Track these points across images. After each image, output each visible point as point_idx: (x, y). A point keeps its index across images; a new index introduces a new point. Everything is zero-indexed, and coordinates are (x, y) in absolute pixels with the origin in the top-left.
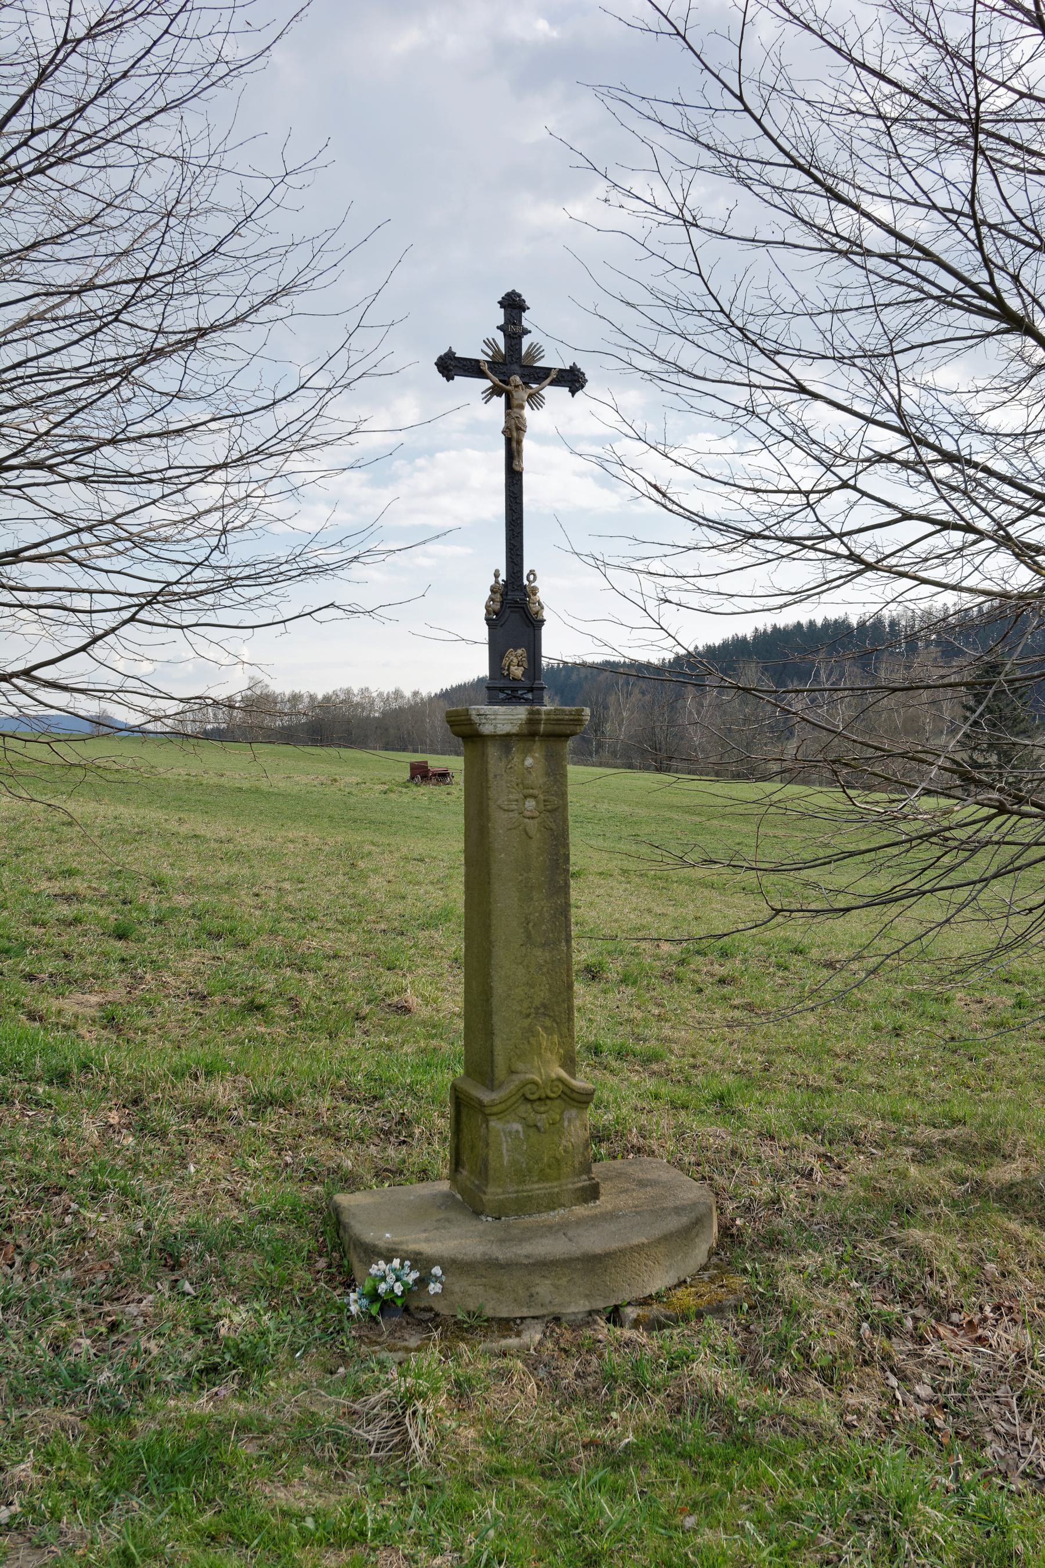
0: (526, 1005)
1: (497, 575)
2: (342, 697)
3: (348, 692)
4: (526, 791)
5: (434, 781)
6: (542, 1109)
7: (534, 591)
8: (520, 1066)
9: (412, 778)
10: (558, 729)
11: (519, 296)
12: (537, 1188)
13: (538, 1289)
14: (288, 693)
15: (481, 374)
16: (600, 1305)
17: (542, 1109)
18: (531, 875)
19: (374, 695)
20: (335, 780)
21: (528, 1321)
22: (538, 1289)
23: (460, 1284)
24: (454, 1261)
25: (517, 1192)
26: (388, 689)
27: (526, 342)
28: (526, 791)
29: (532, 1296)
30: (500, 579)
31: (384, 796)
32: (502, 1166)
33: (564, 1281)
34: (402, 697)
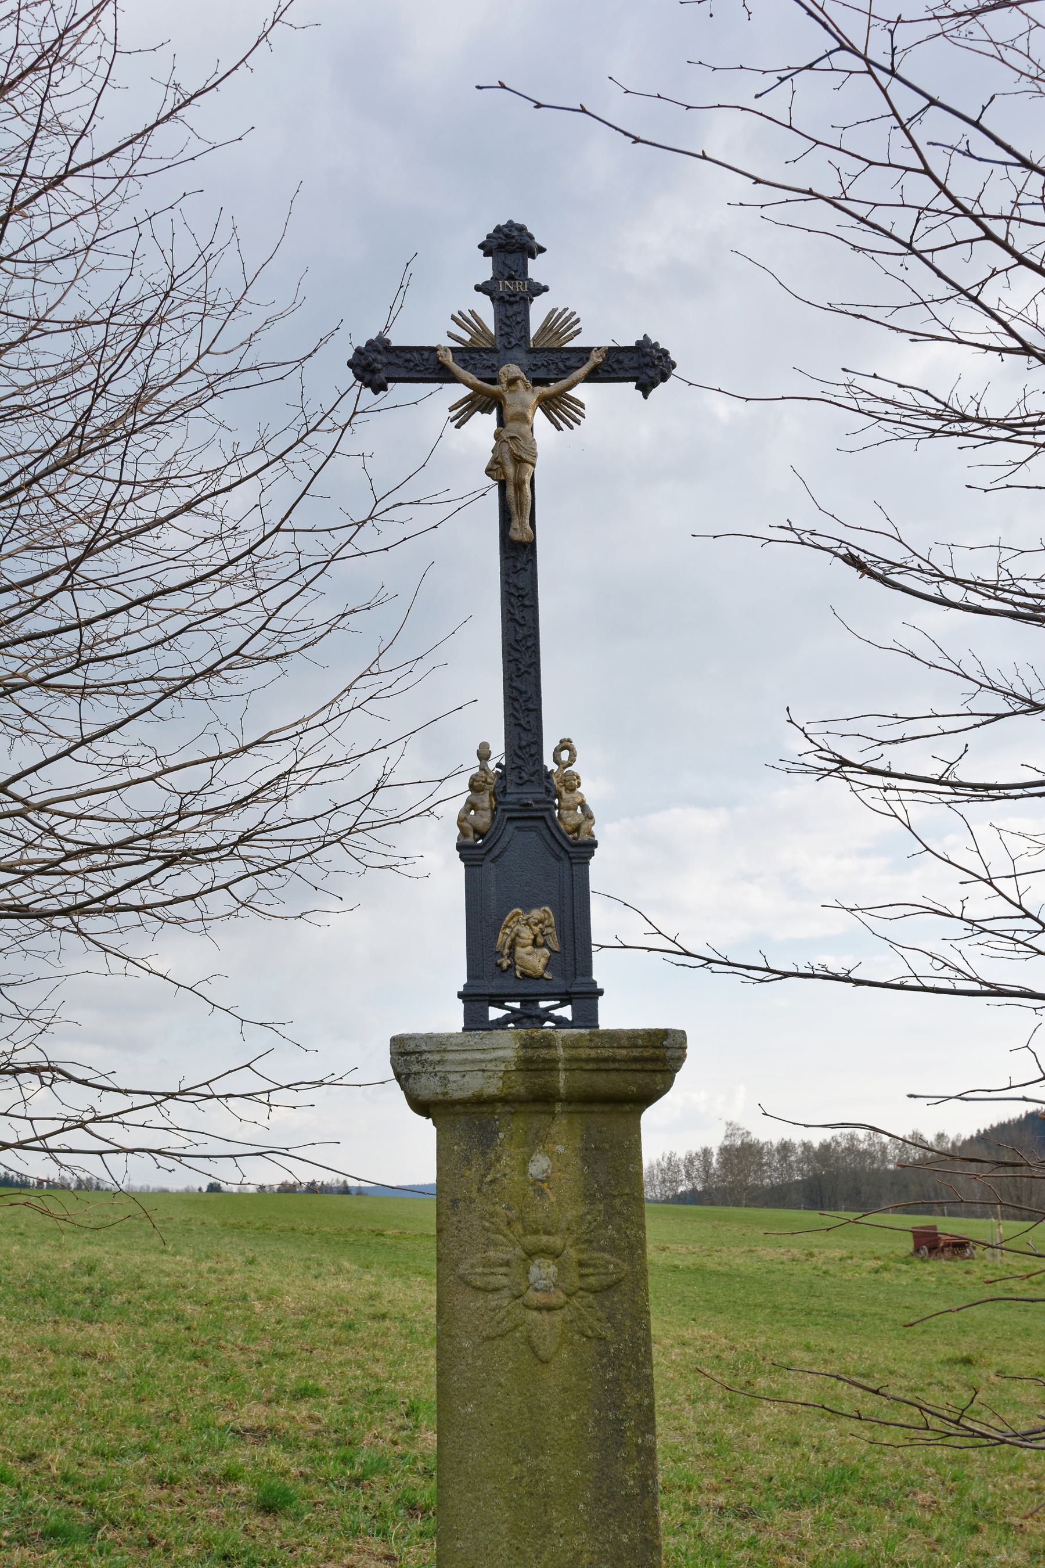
1: (484, 754)
2: (844, 1144)
4: (530, 1240)
5: (948, 1254)
7: (571, 783)
9: (917, 1250)
10: (603, 1082)
11: (522, 229)
14: (776, 1142)
15: (444, 375)
20: (811, 1255)
27: (538, 312)
28: (530, 1240)
30: (491, 765)
31: (873, 1276)
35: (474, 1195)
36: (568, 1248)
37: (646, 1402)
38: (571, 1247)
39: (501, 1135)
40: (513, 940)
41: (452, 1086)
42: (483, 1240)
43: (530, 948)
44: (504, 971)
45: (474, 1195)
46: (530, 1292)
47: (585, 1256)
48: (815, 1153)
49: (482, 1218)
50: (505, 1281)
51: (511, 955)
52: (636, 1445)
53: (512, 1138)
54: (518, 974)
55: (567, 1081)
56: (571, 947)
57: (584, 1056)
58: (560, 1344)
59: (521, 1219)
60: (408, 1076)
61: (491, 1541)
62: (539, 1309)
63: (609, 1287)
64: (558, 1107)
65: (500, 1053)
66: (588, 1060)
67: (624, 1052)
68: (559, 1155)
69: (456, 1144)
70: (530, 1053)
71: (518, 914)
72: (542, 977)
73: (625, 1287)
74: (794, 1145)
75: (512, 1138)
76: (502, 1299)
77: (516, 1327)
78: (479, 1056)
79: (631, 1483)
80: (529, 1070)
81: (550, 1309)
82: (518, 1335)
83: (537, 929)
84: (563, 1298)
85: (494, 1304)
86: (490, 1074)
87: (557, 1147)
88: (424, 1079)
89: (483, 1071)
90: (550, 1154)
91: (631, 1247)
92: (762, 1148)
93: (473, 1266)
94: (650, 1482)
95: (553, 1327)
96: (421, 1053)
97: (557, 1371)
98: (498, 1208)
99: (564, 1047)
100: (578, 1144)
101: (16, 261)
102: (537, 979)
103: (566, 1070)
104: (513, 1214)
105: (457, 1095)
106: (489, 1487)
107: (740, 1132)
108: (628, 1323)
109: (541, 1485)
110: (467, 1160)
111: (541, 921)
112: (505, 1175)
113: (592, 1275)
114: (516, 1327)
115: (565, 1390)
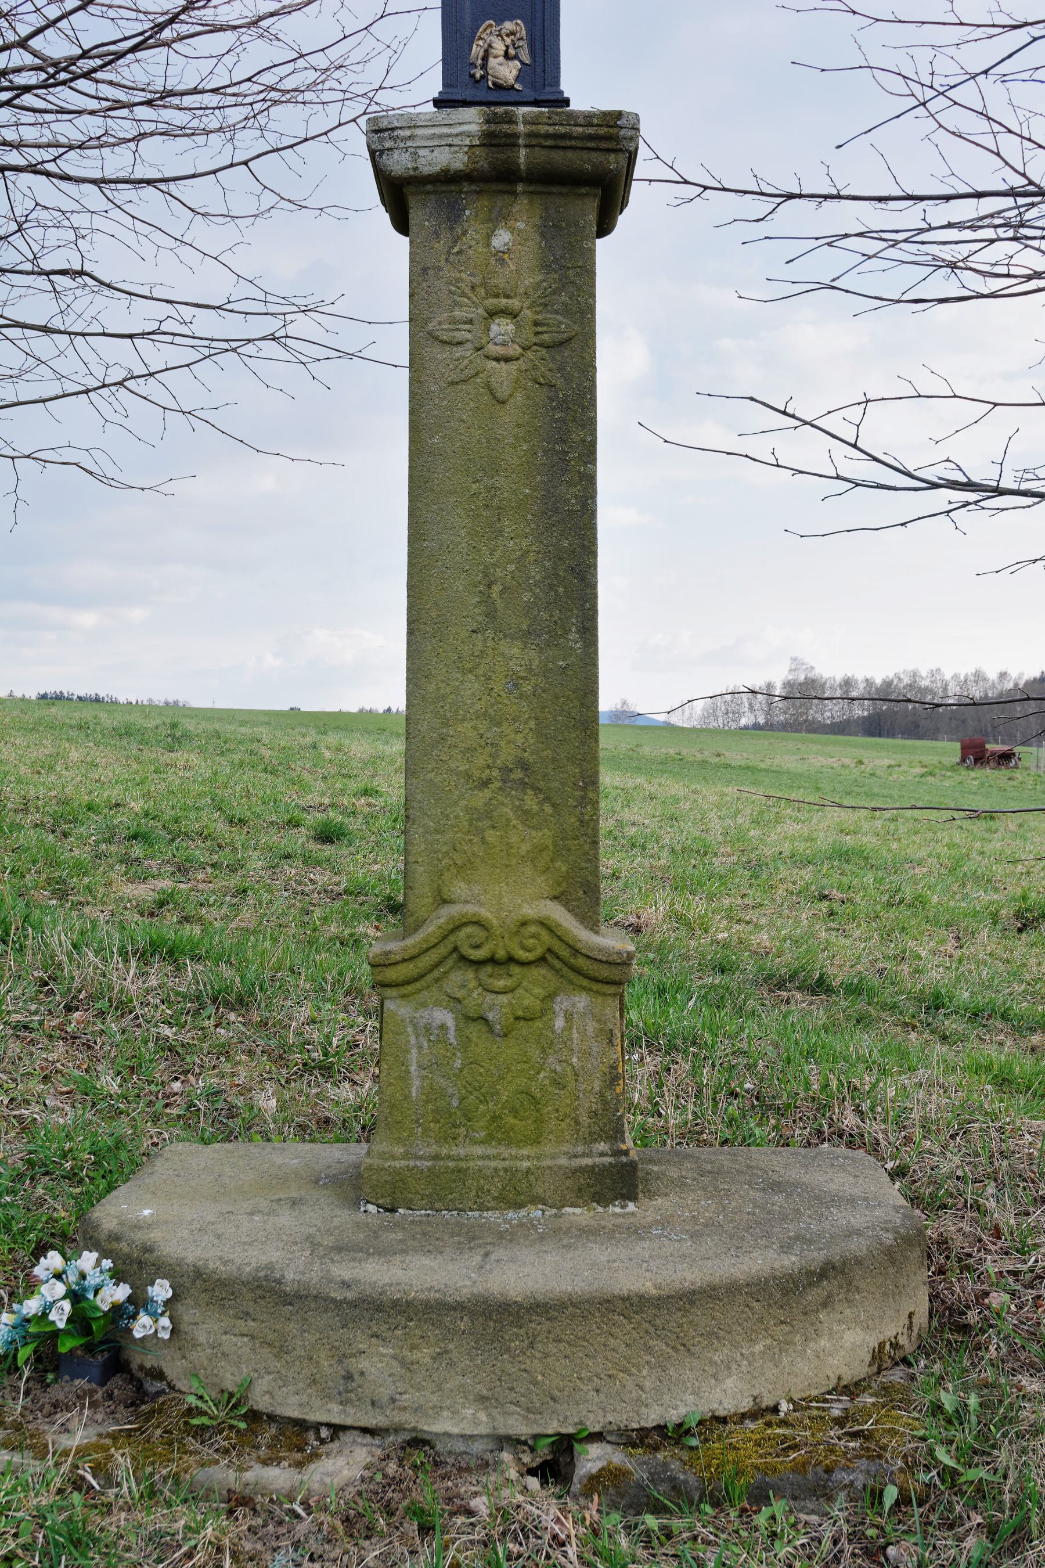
0: (481, 760)
2: (906, 681)
3: (915, 674)
6: (501, 984)
8: (459, 888)
12: (475, 1153)
13: (363, 1364)
16: (520, 1428)
17: (501, 984)
18: (500, 481)
19: (948, 677)
21: (347, 1437)
22: (363, 1364)
23: (207, 1327)
24: (198, 1273)
25: (436, 1157)
26: (966, 670)
29: (349, 1377)
32: (406, 1097)
33: (424, 1355)
34: (985, 679)
35: (442, 264)
36: (525, 310)
37: (589, 438)
38: (528, 308)
39: (468, 212)
40: (486, 51)
41: (422, 161)
42: (450, 302)
43: (501, 59)
44: (477, 82)
45: (442, 264)
46: (490, 346)
47: (540, 317)
48: (877, 689)
49: (449, 283)
50: (468, 336)
51: (484, 66)
52: (579, 472)
53: (477, 216)
54: (490, 83)
55: (527, 156)
56: (541, 60)
57: (542, 132)
58: (515, 389)
59: (484, 284)
60: (382, 152)
61: (452, 542)
62: (497, 360)
63: (561, 344)
64: (520, 188)
65: (465, 128)
66: (547, 136)
67: (580, 129)
68: (520, 231)
69: (427, 220)
70: (493, 127)
71: (491, 25)
72: (512, 87)
73: (575, 345)
74: (856, 682)
75: (477, 216)
76: (466, 351)
77: (477, 374)
78: (446, 130)
79: (573, 501)
80: (492, 145)
81: (507, 360)
82: (479, 380)
83: (508, 41)
84: (519, 350)
85: (458, 355)
86: (456, 149)
87: (518, 224)
88: (396, 155)
89: (450, 145)
90: (511, 230)
91: (582, 312)
92: (825, 683)
93: (440, 323)
94: (590, 502)
95: (510, 374)
96: (393, 129)
97: (513, 411)
98: (463, 275)
99: (525, 123)
100: (537, 221)
101: (97, 81)
102: (508, 89)
103: (526, 146)
104: (477, 280)
105: (426, 170)
106: (452, 500)
107: (804, 667)
108: (576, 374)
109: (496, 499)
110: (437, 234)
111: (512, 33)
112: (470, 247)
113: (546, 332)
114: (477, 374)
115: (518, 426)
